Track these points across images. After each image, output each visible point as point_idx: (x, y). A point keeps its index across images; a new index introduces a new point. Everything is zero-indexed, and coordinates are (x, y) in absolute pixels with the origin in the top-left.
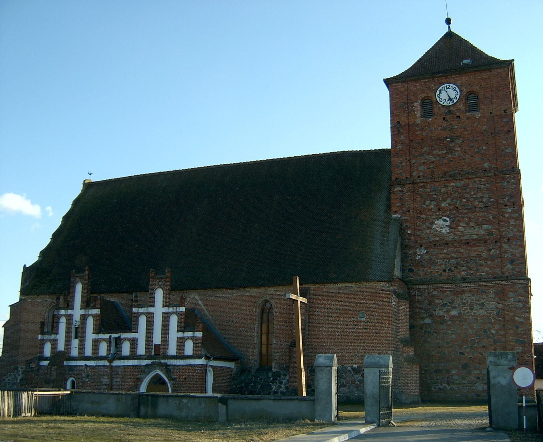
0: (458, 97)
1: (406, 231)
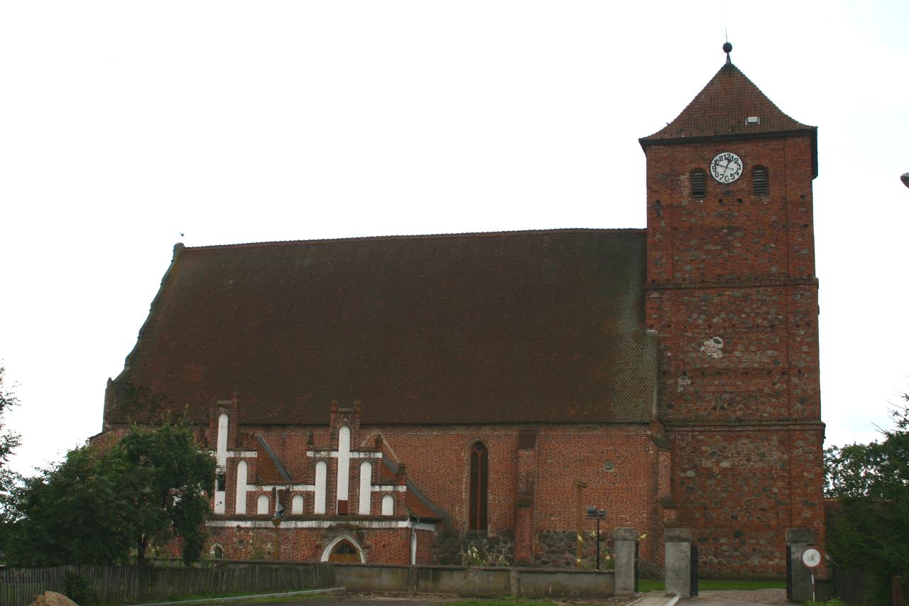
0: (740, 172)
1: (665, 353)
